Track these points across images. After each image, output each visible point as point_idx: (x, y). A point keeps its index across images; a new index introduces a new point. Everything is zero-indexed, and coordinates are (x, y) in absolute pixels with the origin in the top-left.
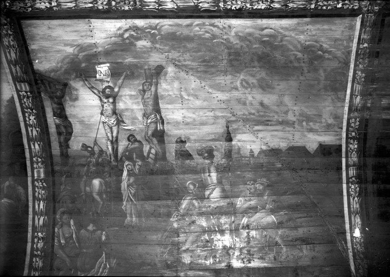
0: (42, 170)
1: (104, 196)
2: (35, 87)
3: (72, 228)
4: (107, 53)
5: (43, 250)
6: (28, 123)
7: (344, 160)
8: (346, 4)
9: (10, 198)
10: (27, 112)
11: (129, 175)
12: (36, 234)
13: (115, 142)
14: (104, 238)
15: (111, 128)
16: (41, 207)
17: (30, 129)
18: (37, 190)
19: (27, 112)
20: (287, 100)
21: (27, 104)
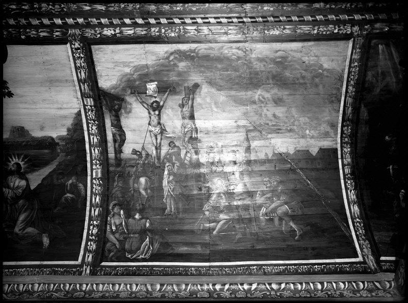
0: (99, 171)
1: (149, 191)
2: (98, 102)
3: (122, 217)
4: (157, 73)
5: (97, 235)
6: (90, 132)
7: (340, 161)
8: (341, 30)
9: (72, 193)
10: (90, 123)
11: (169, 174)
12: (92, 222)
14: (148, 225)
15: (156, 136)
16: (97, 200)
17: (92, 137)
18: (94, 186)
19: (90, 123)
20: (294, 111)
21: (91, 116)
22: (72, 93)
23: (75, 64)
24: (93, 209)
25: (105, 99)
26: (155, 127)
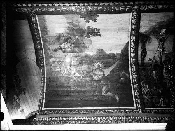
0: (134, 68)
5: (139, 96)
9: (124, 78)
11: (166, 69)
13: (161, 58)
16: (135, 81)
17: (131, 54)
22: (127, 34)
23: (132, 21)
24: (134, 85)
25: (141, 37)
26: (160, 49)
